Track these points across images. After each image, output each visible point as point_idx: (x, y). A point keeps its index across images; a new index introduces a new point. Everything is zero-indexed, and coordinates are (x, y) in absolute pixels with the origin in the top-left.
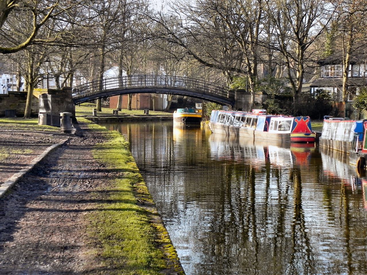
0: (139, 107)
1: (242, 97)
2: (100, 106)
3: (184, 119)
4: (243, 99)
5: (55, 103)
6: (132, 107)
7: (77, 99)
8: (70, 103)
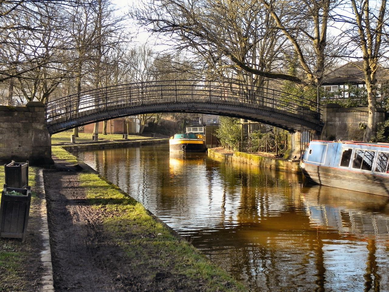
0: (113, 131)
1: (335, 116)
2: (77, 131)
3: (183, 147)
4: (337, 119)
5: (11, 132)
6: (107, 132)
7: (55, 124)
8: (40, 131)
